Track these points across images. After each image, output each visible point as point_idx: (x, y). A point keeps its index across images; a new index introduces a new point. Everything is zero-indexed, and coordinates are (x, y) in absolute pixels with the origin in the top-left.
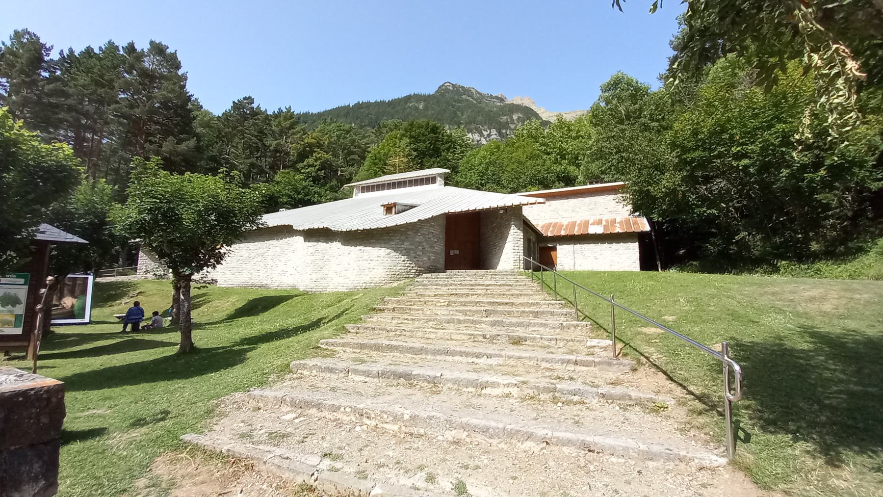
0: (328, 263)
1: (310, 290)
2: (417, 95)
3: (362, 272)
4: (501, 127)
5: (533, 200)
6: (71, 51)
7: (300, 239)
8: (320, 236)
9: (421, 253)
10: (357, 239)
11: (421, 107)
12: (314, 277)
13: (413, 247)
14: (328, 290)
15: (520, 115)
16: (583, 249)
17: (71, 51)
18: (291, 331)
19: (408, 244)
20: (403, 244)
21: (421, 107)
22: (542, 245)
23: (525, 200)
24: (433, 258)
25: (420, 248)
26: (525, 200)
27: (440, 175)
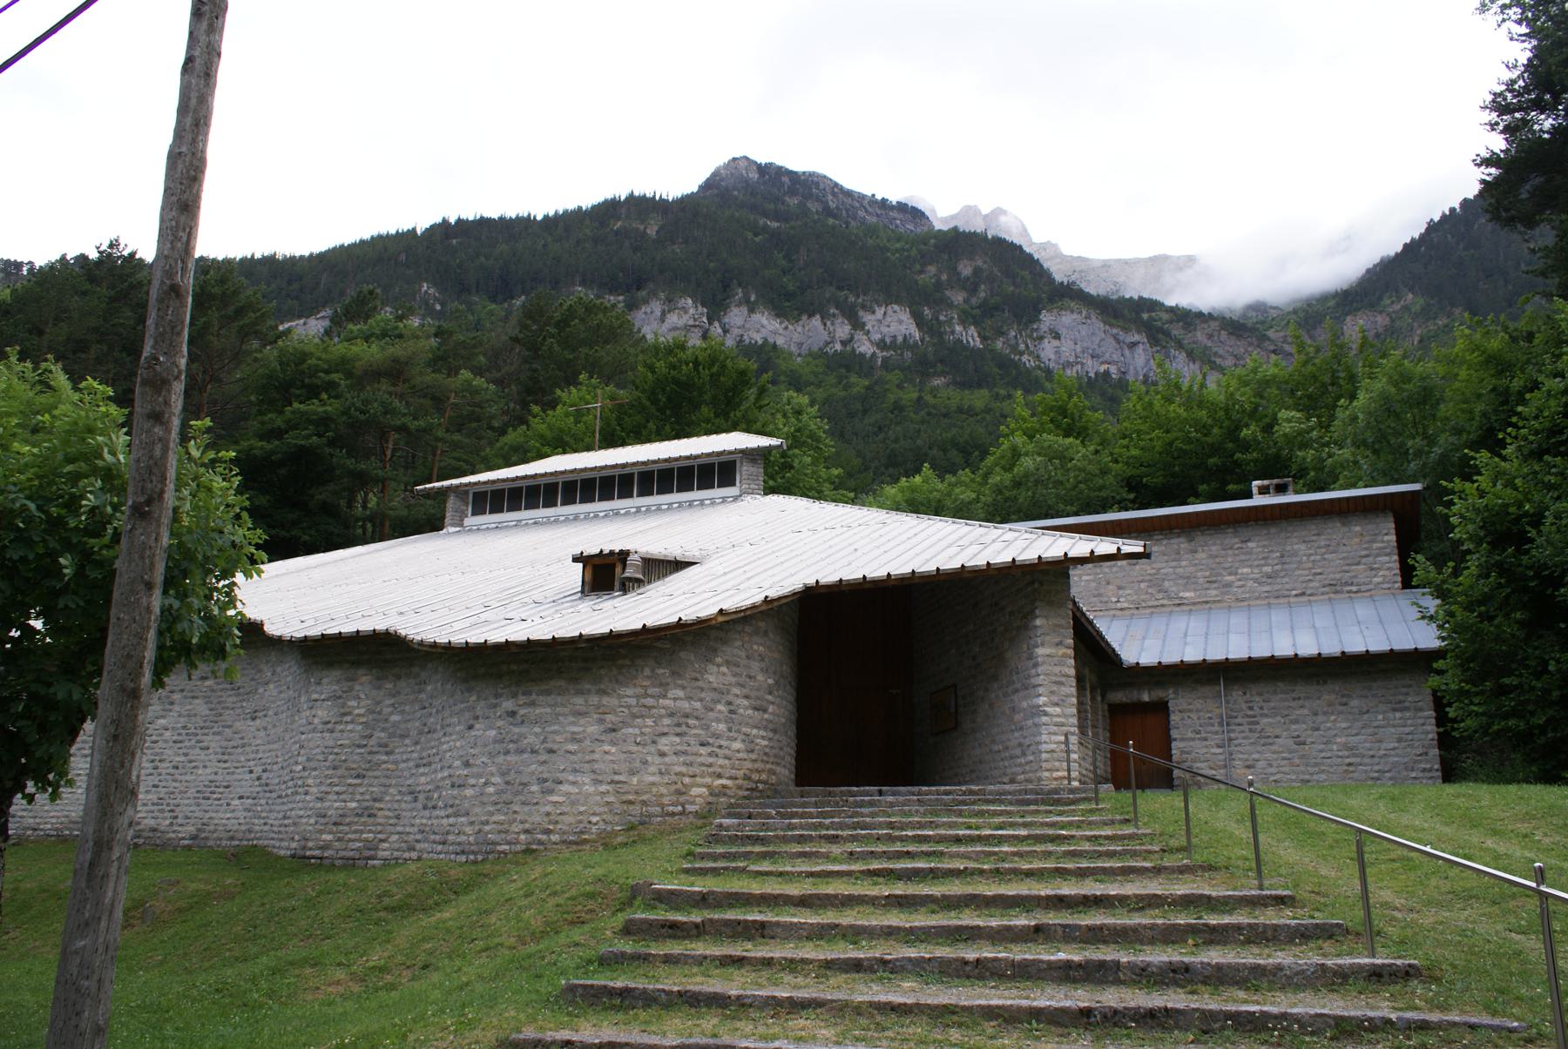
0: (384, 758)
1: (317, 853)
2: (643, 198)
3: (517, 793)
4: (918, 300)
5: (1106, 546)
6: (253, 256)
7: (289, 670)
8: (356, 664)
9: (722, 727)
10: (500, 676)
11: (652, 231)
12: (334, 806)
13: (697, 705)
14: (381, 854)
15: (980, 263)
16: (1257, 711)
17: (253, 256)
18: (33, 842)
19: (680, 693)
20: (665, 697)
21: (652, 231)
22: (1119, 697)
23: (1080, 546)
24: (765, 743)
25: (720, 707)
26: (1080, 546)
27: (749, 454)
